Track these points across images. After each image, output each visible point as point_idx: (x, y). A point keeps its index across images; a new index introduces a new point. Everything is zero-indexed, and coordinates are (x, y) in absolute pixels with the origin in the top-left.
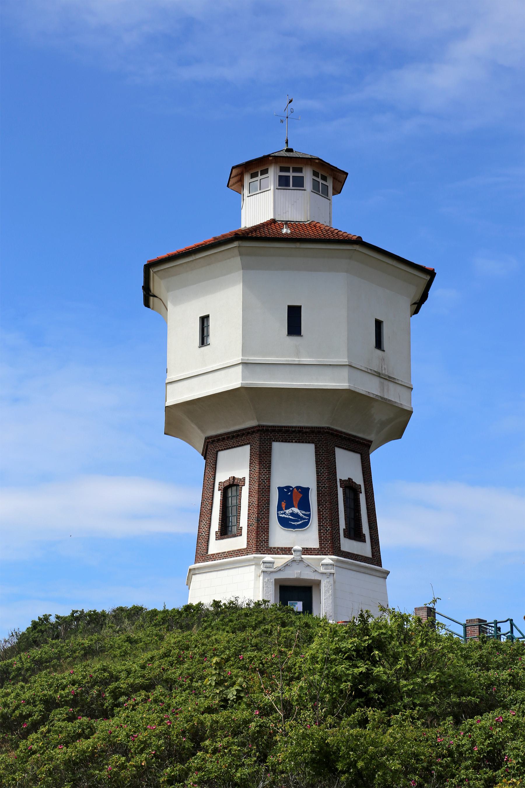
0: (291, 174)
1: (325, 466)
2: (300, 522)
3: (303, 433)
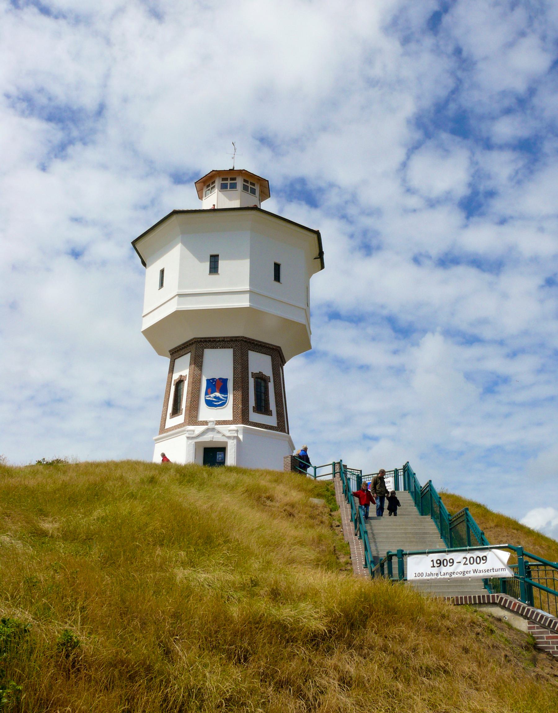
1: (241, 365)
3: (225, 342)
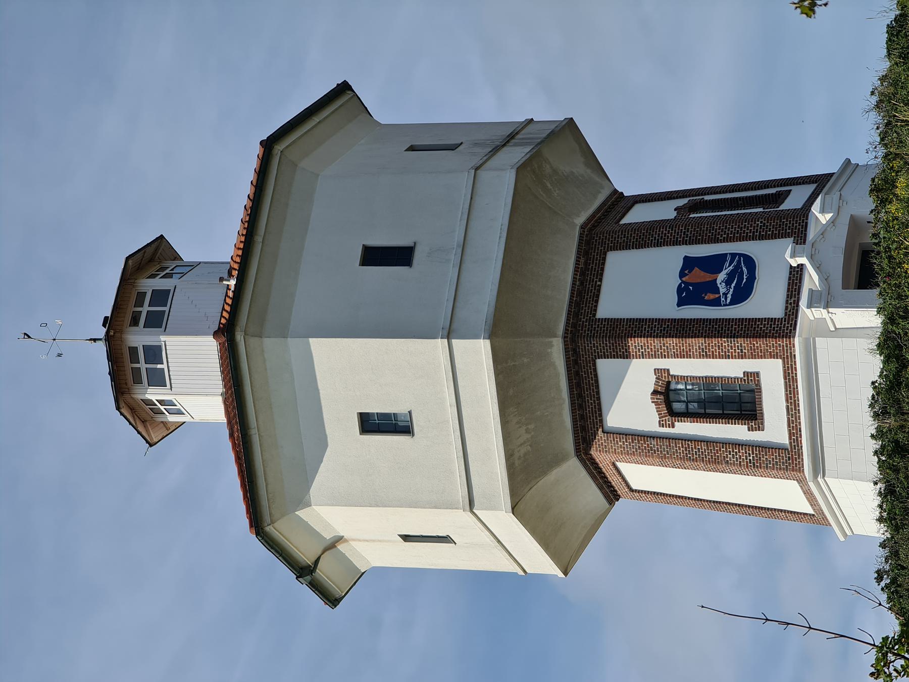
2: (744, 269)
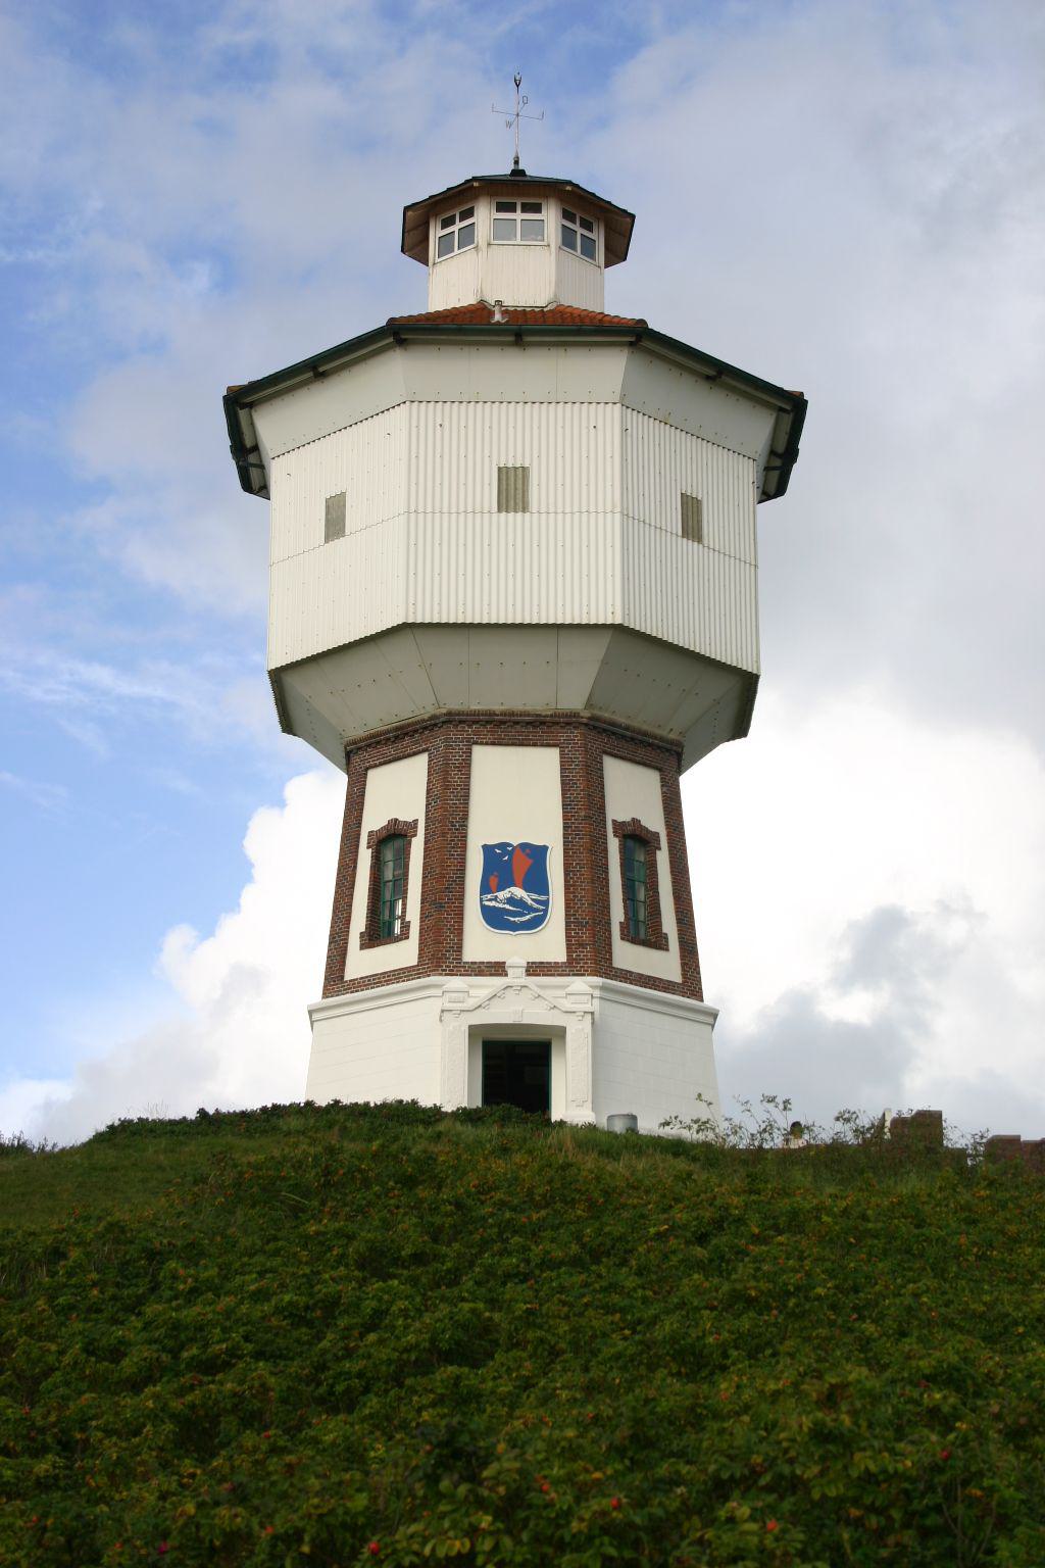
0: (519, 216)
1: (583, 802)
2: (528, 917)
